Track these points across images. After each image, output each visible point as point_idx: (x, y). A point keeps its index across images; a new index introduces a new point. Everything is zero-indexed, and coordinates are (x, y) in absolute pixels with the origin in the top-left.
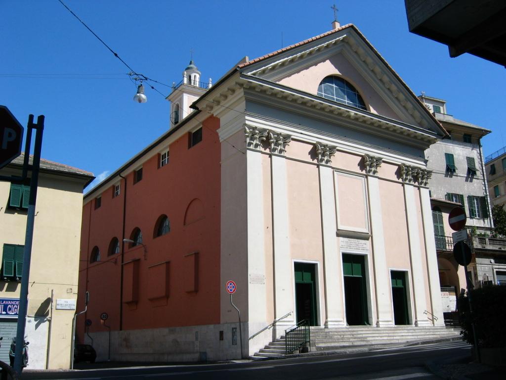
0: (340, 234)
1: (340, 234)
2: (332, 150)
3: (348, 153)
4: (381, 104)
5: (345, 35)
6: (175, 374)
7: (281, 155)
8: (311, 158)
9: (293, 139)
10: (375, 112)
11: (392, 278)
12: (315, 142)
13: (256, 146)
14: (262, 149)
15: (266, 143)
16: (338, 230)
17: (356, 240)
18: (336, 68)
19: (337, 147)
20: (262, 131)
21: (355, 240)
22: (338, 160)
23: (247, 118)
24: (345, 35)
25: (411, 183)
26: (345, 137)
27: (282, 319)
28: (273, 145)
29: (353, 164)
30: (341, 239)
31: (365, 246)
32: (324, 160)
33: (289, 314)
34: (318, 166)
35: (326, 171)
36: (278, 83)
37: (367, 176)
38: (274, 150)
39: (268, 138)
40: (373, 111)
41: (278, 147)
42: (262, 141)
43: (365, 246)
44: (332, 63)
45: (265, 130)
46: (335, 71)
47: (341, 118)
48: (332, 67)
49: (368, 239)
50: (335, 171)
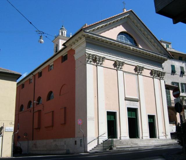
0: (126, 99)
3: (129, 65)
10: (141, 48)
13: (91, 62)
14: (93, 63)
15: (95, 60)
20: (158, 71)
22: (125, 68)
23: (86, 50)
25: (91, 63)
27: (101, 135)
30: (127, 101)
32: (119, 68)
39: (96, 58)
40: (140, 47)
42: (93, 60)
46: (124, 30)
49: (138, 101)
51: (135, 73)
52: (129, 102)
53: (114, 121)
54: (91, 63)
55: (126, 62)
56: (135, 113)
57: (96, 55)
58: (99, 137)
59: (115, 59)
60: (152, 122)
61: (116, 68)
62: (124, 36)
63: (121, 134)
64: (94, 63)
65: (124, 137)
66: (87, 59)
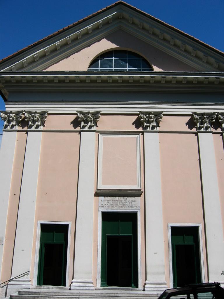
0: (98, 193)
1: (98, 193)
2: (96, 115)
3: (118, 115)
4: (165, 60)
5: (116, 13)
6: (206, 298)
7: (154, 130)
8: (189, 128)
9: (102, 114)
10: (161, 70)
11: (172, 235)
12: (191, 113)
13: (207, 128)
14: (213, 130)
15: (23, 123)
16: (97, 189)
17: (122, 198)
18: (113, 43)
19: (163, 112)
20: (210, 115)
21: (120, 198)
22: (166, 123)
23: (6, 106)
24: (116, 13)
25: (209, 130)
26: (177, 101)
27: (17, 277)
28: (198, 125)
29: (181, 123)
30: (102, 198)
31: (133, 203)
32: (203, 127)
33: (26, 274)
34: (197, 134)
35: (89, 138)
36: (44, 71)
37: (143, 133)
38: (200, 128)
39: (217, 119)
40: (156, 69)
41: (204, 124)
42: (212, 124)
43: (133, 203)
44: (108, 40)
45: (214, 113)
46: (113, 46)
47: (76, 84)
48: (109, 43)
49: (139, 195)
50: (101, 134)
51: (135, 130)
52: (108, 198)
53: (62, 245)
54: (209, 130)
55: (166, 111)
56: (131, 223)
57: (218, 113)
58: (146, 286)
59: (190, 112)
60: (192, 243)
61: (194, 130)
62: (113, 59)
63: (210, 279)
64: (216, 130)
65: (81, 284)
66: (5, 123)
